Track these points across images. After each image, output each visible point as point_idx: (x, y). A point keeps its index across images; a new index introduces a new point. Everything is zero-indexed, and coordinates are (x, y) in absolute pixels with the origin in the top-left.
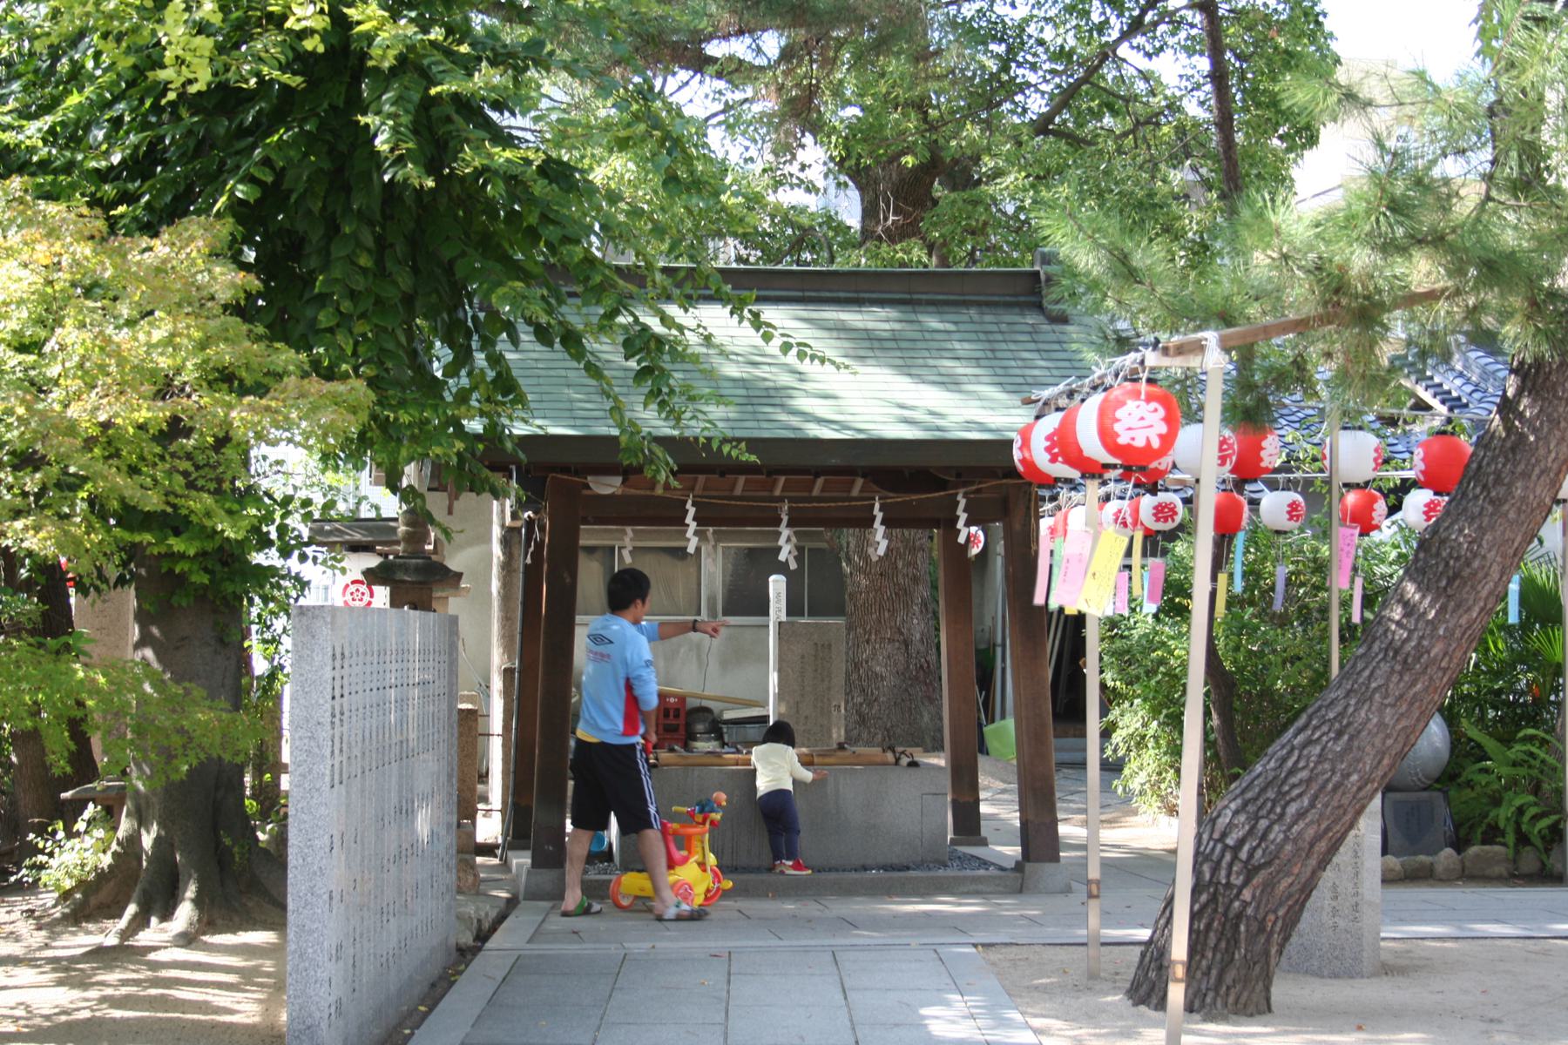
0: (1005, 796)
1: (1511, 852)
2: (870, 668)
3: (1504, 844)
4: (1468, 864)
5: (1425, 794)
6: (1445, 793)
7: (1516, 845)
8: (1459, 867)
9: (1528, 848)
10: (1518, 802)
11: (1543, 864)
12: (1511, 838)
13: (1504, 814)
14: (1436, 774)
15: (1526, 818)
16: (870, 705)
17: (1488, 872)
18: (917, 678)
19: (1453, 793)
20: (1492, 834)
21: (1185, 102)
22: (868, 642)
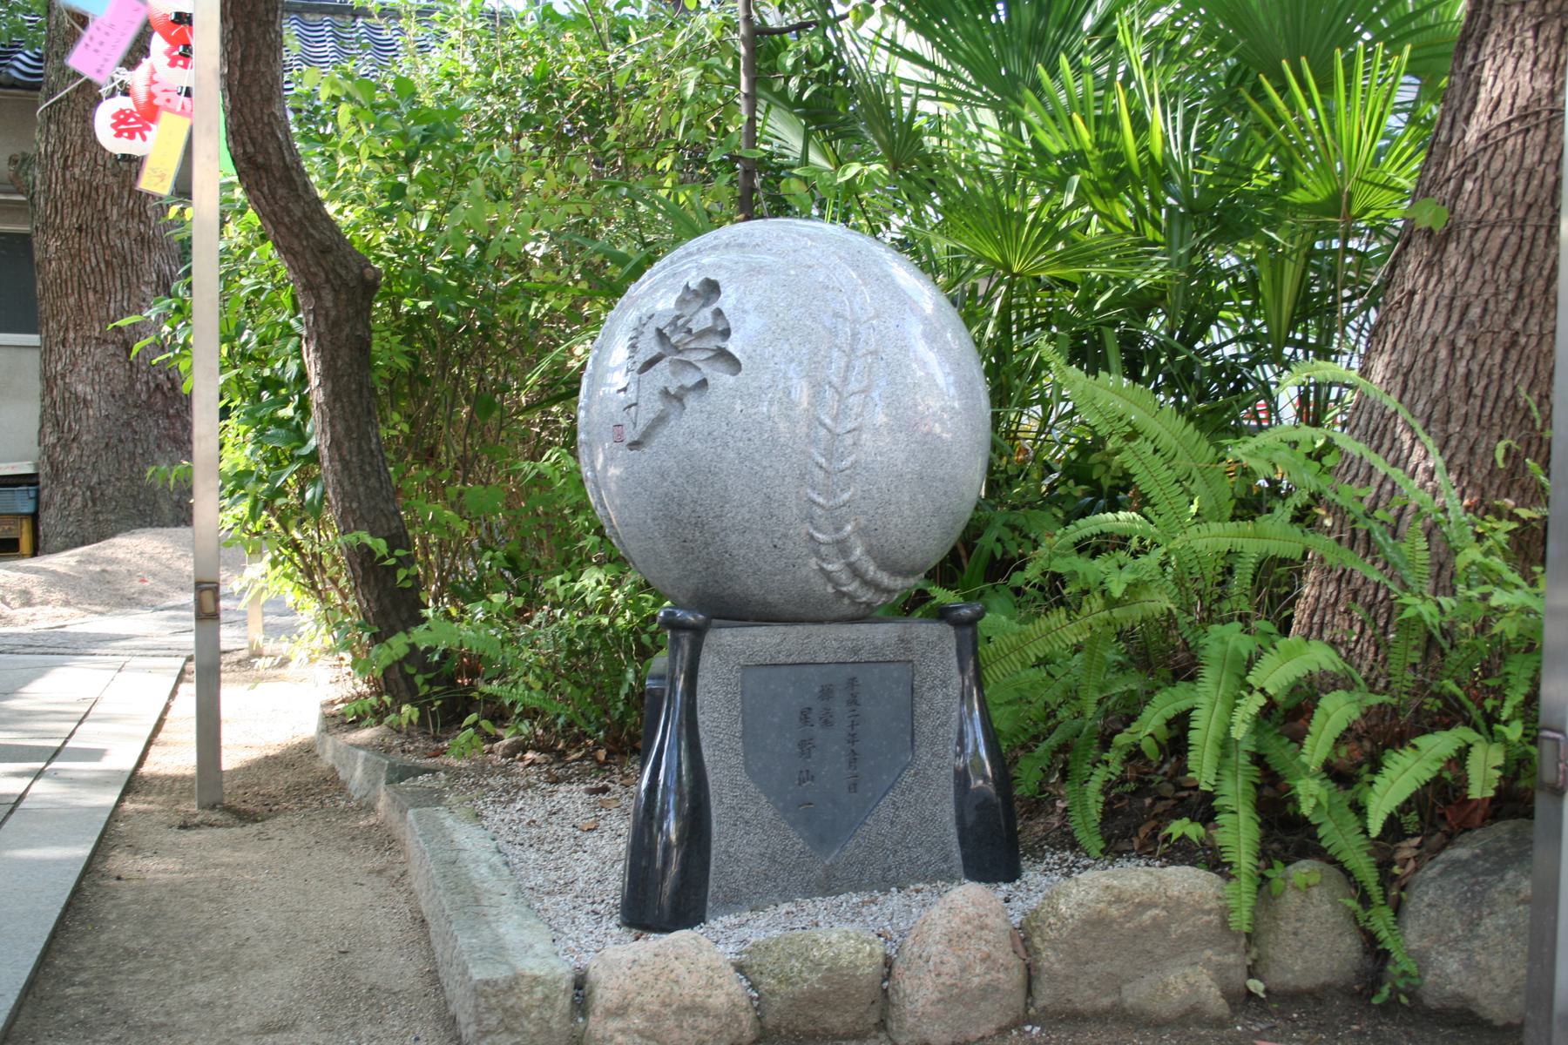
0: (182, 613)
1: (1242, 894)
2: (67, 387)
3: (1216, 863)
4: (1050, 959)
5: (882, 634)
6: (966, 626)
7: (1265, 855)
8: (1012, 979)
9: (1304, 871)
10: (1277, 673)
11: (1370, 941)
12: (1239, 832)
13: (1218, 718)
14: (933, 546)
15: (1318, 746)
16: (67, 448)
17: (1136, 994)
18: (149, 405)
19: (998, 621)
20: (1151, 808)
21: (1202, 830)
22: (64, 342)
